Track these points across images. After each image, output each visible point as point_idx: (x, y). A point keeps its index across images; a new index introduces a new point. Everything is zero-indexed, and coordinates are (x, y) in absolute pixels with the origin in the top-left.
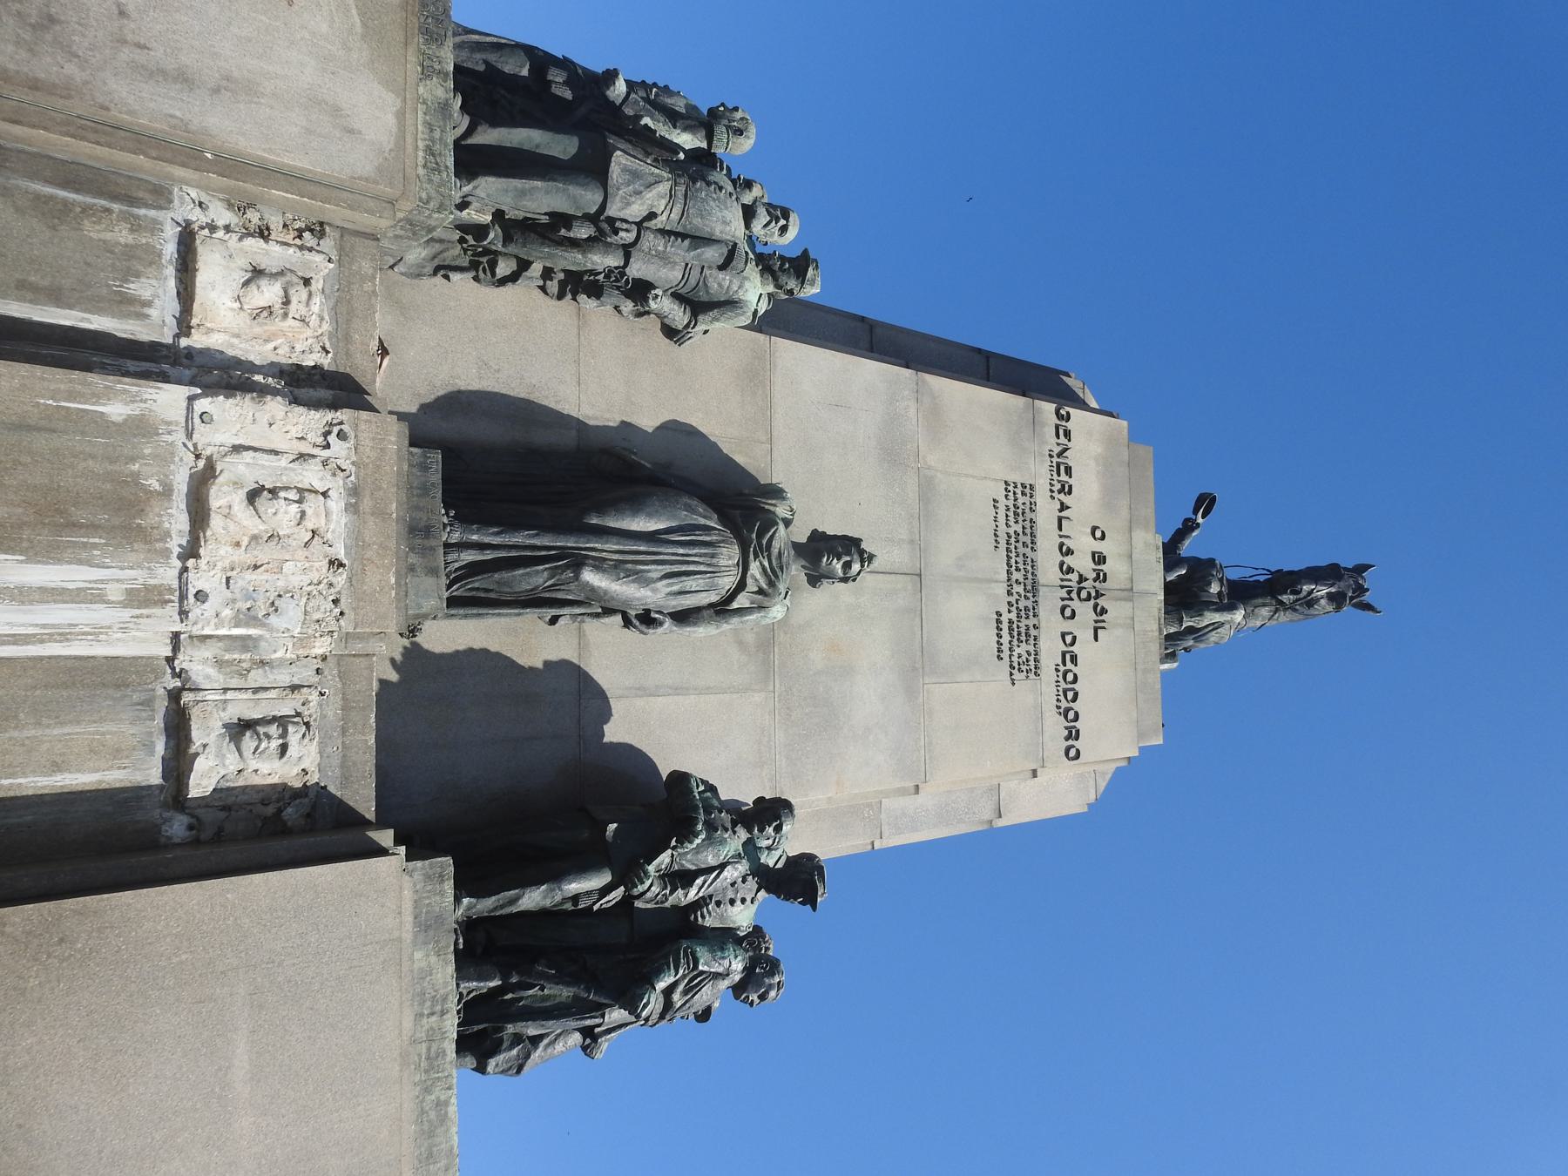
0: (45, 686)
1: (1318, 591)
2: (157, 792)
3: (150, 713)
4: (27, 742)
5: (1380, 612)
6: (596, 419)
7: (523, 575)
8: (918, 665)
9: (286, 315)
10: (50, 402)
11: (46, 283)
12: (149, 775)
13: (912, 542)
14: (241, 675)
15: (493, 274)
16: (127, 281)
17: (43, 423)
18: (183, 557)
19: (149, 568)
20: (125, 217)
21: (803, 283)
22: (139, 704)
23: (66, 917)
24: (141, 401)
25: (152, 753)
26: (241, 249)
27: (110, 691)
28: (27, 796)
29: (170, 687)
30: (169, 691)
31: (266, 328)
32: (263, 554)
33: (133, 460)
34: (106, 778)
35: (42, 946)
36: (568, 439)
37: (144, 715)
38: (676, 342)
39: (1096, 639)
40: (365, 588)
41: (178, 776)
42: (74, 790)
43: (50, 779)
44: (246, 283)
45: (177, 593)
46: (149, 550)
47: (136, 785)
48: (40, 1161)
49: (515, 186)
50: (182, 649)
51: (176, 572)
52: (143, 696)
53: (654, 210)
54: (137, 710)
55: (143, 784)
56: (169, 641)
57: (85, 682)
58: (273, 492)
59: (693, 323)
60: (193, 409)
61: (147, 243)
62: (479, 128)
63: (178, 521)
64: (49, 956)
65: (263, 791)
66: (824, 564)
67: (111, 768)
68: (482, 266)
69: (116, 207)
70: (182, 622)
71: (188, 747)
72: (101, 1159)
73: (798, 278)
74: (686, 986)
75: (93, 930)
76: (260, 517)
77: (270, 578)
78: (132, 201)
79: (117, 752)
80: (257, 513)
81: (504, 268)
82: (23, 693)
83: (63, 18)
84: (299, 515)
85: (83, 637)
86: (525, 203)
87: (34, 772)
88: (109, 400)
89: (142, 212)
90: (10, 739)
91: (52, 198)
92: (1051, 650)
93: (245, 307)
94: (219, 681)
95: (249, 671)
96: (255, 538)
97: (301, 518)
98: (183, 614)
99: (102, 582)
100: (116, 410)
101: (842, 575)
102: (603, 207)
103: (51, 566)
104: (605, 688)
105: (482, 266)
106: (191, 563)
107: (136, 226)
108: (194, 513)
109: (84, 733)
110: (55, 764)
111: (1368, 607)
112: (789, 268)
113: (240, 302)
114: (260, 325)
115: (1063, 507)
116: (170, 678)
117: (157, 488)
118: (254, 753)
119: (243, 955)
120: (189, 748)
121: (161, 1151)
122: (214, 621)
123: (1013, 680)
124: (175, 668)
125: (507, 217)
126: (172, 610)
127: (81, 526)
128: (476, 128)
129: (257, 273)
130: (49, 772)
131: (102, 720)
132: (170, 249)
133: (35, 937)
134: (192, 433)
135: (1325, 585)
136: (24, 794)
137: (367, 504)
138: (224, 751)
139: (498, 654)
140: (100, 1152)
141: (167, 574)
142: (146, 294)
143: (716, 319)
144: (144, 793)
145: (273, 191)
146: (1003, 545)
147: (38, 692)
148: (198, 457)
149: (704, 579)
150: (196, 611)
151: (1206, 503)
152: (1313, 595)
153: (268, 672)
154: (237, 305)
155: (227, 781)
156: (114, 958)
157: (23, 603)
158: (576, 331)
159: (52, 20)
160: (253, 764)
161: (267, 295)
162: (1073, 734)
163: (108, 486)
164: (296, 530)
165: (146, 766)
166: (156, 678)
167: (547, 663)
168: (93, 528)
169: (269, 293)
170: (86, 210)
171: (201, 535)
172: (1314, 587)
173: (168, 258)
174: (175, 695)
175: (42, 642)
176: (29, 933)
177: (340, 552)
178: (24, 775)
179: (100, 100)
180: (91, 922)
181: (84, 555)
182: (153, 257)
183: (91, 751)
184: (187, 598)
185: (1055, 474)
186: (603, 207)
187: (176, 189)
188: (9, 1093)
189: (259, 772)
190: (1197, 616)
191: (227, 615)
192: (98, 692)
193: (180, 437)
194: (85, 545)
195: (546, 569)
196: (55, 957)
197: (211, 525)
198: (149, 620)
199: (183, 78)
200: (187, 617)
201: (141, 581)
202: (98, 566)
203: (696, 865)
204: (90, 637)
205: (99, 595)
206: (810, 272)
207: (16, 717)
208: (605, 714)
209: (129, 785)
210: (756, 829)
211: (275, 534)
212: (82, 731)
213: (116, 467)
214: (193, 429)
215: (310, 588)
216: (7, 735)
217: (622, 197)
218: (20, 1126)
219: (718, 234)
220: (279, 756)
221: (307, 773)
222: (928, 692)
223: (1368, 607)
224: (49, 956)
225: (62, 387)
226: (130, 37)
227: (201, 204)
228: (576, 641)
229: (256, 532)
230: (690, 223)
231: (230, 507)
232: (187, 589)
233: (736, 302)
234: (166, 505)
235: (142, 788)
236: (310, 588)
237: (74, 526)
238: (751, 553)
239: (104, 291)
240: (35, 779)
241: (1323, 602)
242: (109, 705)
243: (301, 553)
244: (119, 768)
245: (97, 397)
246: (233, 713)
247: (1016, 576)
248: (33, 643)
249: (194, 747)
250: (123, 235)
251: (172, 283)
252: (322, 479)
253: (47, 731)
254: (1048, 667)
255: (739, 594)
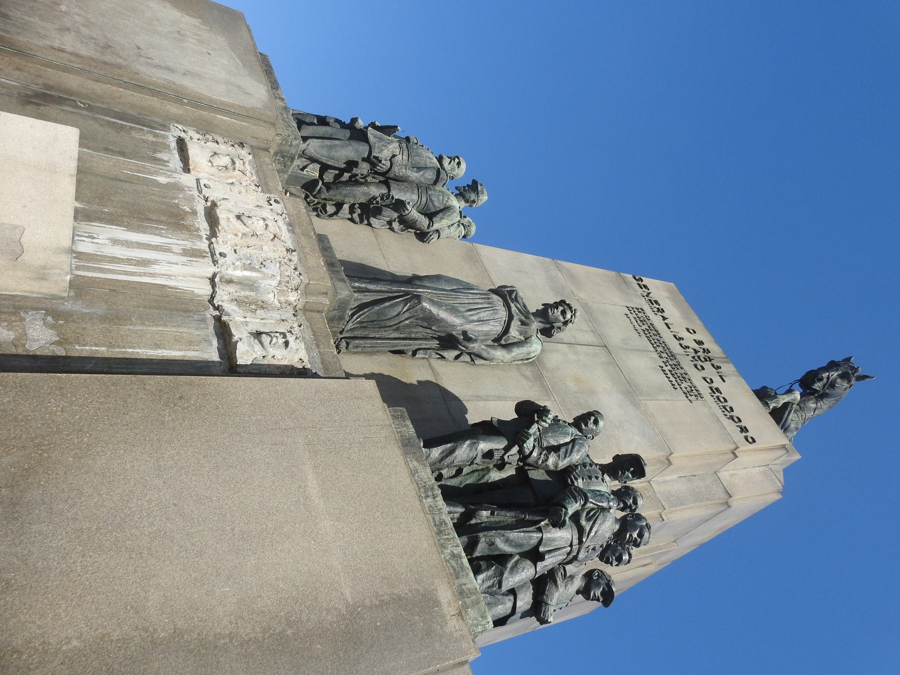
0: (144, 307)
1: (832, 376)
2: (218, 365)
3: (206, 326)
4: (138, 332)
5: (873, 377)
6: (399, 272)
7: (389, 306)
8: (631, 390)
9: (234, 169)
10: (129, 172)
11: (118, 149)
12: (211, 356)
13: (592, 331)
14: (252, 311)
15: (326, 212)
16: (155, 153)
17: (126, 179)
18: (209, 239)
19: (192, 241)
20: (151, 133)
21: (478, 194)
22: (198, 321)
23: (181, 385)
24: (173, 177)
25: (211, 345)
26: (207, 146)
27: (181, 313)
28: (143, 359)
29: (214, 314)
30: (214, 316)
31: (226, 174)
32: (252, 241)
33: (175, 198)
34: (187, 355)
35: (170, 399)
37: (202, 326)
38: (426, 241)
39: (724, 381)
40: (309, 264)
41: (229, 357)
42: (169, 359)
43: (154, 351)
45: (209, 254)
46: (191, 234)
47: (205, 360)
48: (193, 530)
49: (327, 145)
50: (217, 286)
51: (207, 245)
52: (200, 317)
53: (395, 154)
54: (198, 323)
55: (209, 360)
56: (209, 284)
57: (166, 307)
59: (431, 223)
60: (199, 182)
61: (162, 142)
62: (303, 127)
64: (175, 405)
65: (280, 368)
66: (551, 314)
67: (189, 350)
68: (319, 209)
69: (145, 128)
70: (215, 265)
71: (231, 339)
72: (234, 535)
73: (475, 192)
74: (586, 517)
75: (199, 394)
76: (245, 225)
77: (257, 252)
78: (152, 128)
79: (190, 343)
80: (243, 223)
81: (331, 209)
82: (133, 309)
83: (114, 46)
84: (265, 226)
85: (162, 276)
86: (333, 153)
87: (145, 347)
88: (158, 175)
89: (158, 131)
90: (129, 329)
91: (115, 122)
93: (214, 164)
94: (240, 313)
95: (256, 310)
96: (244, 234)
97: (266, 227)
99: (169, 244)
101: (563, 320)
102: (370, 152)
103: (140, 234)
104: (457, 395)
105: (319, 209)
106: (213, 240)
107: (156, 135)
108: (210, 223)
109: (170, 331)
110: (156, 344)
111: (864, 377)
112: (468, 189)
113: (211, 162)
114: (223, 173)
115: (664, 319)
116: (213, 310)
117: (189, 210)
118: (270, 344)
119: (295, 421)
120: (232, 339)
121: (275, 536)
122: (232, 266)
123: (690, 400)
124: (214, 304)
125: (325, 182)
126: (209, 260)
127: (153, 220)
128: (301, 127)
130: (154, 348)
131: (179, 326)
133: (165, 393)
134: (201, 191)
135: (834, 371)
136: (141, 357)
137: (298, 230)
138: (252, 343)
139: (389, 376)
140: (233, 530)
141: (204, 245)
143: (442, 218)
144: (211, 364)
145: (218, 116)
147: (140, 309)
148: (206, 201)
149: (489, 311)
150: (221, 260)
152: (831, 379)
153: (267, 312)
154: (210, 164)
155: (258, 361)
156: (215, 412)
157: (128, 247)
158: (374, 238)
160: (272, 351)
161: (223, 160)
162: (744, 430)
163: (164, 207)
164: (265, 232)
165: (208, 351)
166: (205, 310)
167: (419, 382)
168: (161, 222)
170: (131, 128)
171: (216, 229)
172: (828, 374)
173: (173, 147)
174: (218, 319)
175: (141, 276)
176: (161, 391)
178: (139, 348)
179: (135, 71)
180: (197, 390)
181: (157, 232)
182: (167, 147)
183: (176, 340)
184: (215, 255)
185: (651, 305)
186: (370, 152)
187: (172, 126)
188: (164, 483)
189: (275, 357)
190: (775, 399)
191: (238, 265)
192: (174, 313)
193: (196, 193)
194: (157, 228)
195: (401, 301)
196: (179, 406)
197: (220, 223)
198: (197, 263)
200: (217, 263)
201: (189, 246)
202: (165, 237)
203: (559, 268)
204: (166, 277)
205: (168, 249)
206: (479, 188)
207: (130, 319)
208: (464, 410)
209: (201, 359)
210: (583, 426)
211: (255, 234)
212: (170, 330)
213: (167, 200)
214: (201, 190)
215: (280, 259)
216: (127, 327)
217: (378, 148)
218: (175, 505)
219: (429, 165)
220: (285, 347)
221: (303, 362)
222: (645, 404)
223: (864, 377)
224: (175, 405)
225: (134, 168)
226: (144, 55)
227: (184, 131)
228: (431, 371)
229: (245, 232)
230: (414, 160)
231: (228, 219)
232: (214, 251)
233: (449, 207)
234: (195, 217)
235: (209, 362)
236: (280, 259)
237: (150, 220)
238: (510, 301)
239: (145, 155)
240: (146, 351)
241: (839, 380)
242: (182, 320)
243: (270, 243)
244: (194, 350)
247: (659, 349)
248: (136, 276)
249: (235, 338)
250: (151, 138)
251: (177, 156)
252: (272, 216)
253: (149, 328)
254: (706, 394)
255: (511, 322)
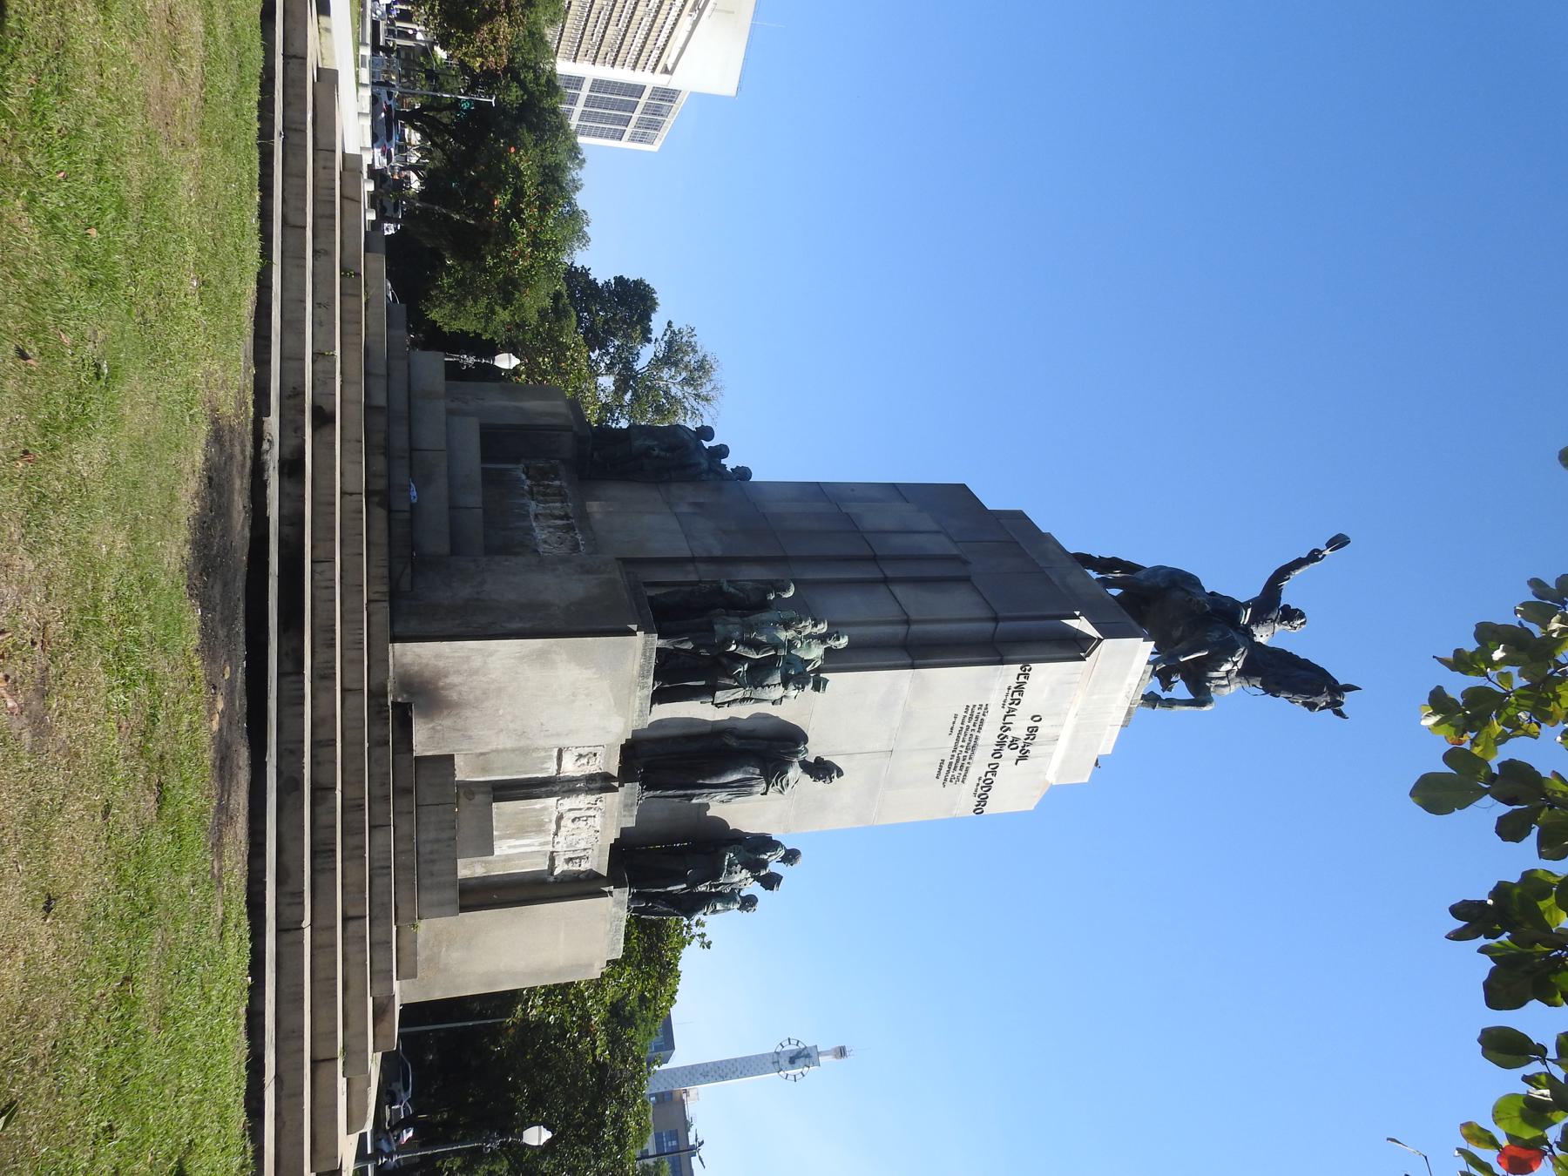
36: (708, 729)
44: (577, 760)
58: (579, 818)
63: (553, 827)
92: (978, 769)
98: (553, 847)
100: (538, 806)
111: (1340, 714)
129: (580, 756)
132: (556, 754)
141: (550, 838)
142: (548, 766)
146: (956, 732)
151: (1338, 542)
159: (524, 732)
169: (584, 761)
177: (598, 828)
199: (558, 735)
237: (527, 832)
245: (533, 804)
246: (567, 857)
